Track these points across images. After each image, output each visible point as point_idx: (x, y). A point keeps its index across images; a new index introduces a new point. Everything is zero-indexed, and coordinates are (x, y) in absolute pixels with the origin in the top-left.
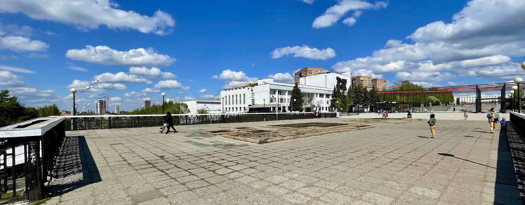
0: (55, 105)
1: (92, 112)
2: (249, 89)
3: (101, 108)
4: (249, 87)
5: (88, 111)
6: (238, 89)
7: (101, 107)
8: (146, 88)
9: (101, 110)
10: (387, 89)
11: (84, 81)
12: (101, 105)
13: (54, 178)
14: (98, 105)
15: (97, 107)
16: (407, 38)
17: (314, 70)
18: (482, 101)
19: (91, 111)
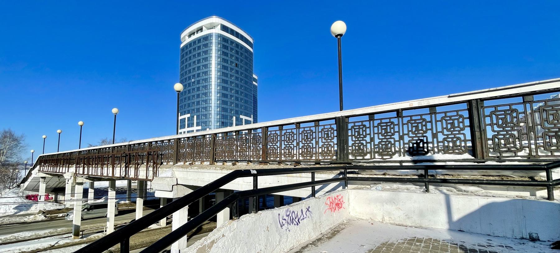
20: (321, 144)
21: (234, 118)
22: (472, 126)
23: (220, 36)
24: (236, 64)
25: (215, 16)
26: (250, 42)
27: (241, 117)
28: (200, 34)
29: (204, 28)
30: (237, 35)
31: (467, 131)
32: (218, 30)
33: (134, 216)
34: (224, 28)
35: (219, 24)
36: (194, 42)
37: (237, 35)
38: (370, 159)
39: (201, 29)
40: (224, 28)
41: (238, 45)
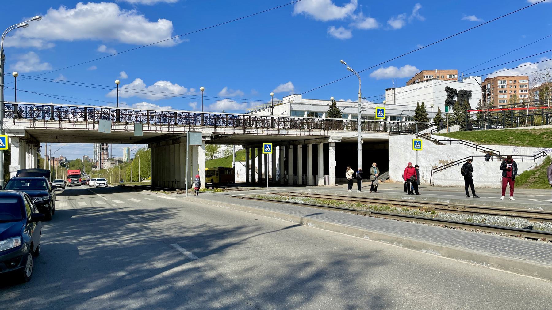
0: (440, 160)
1: (90, 160)
2: (268, 110)
3: (100, 152)
4: (268, 109)
5: (84, 157)
6: (262, 111)
7: (101, 151)
8: (278, 85)
9: (100, 156)
10: (538, 165)
11: (12, 291)
12: (101, 147)
13: (44, 185)
14: (97, 148)
15: (96, 151)
16: (469, 185)
17: (493, 143)
18: (214, 128)
19: (88, 158)
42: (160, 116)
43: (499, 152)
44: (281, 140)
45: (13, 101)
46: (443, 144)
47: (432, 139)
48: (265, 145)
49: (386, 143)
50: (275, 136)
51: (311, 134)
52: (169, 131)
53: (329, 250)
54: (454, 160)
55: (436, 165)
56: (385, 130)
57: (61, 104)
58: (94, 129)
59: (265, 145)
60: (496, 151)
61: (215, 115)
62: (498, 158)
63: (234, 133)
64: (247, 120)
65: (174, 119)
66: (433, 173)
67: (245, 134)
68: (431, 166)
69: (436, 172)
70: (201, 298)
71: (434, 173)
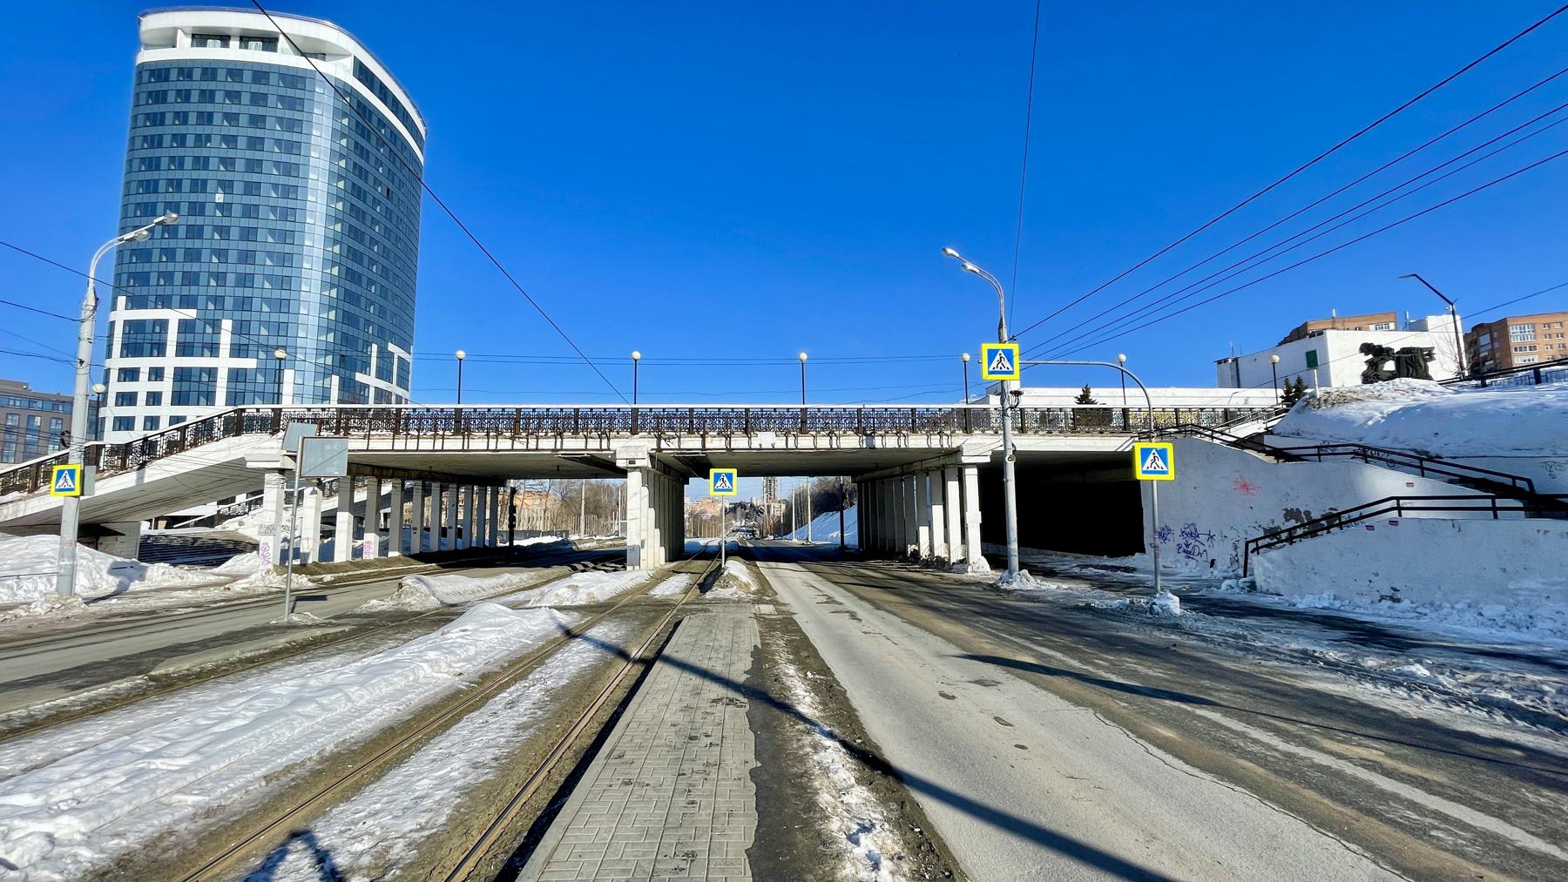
20: (593, 422)
21: (375, 347)
22: (1021, 418)
23: (342, 91)
24: (388, 190)
25: (329, 23)
26: (418, 131)
27: (391, 347)
28: (255, 55)
29: (282, 43)
30: (384, 94)
31: (1020, 420)
32: (341, 71)
33: (1417, 375)
34: (362, 73)
35: (350, 55)
36: (210, 70)
37: (384, 94)
38: (485, 450)
39: (269, 41)
40: (362, 73)
41: (395, 134)
42: (772, 418)
43: (1529, 481)
44: (496, 476)
45: (800, 404)
46: (1298, 458)
47: (1267, 449)
48: (715, 474)
49: (1123, 461)
50: (477, 459)
51: (604, 446)
52: (555, 450)
53: (817, 784)
54: (1336, 510)
55: (1276, 525)
56: (1126, 428)
57: (489, 404)
58: (527, 450)
59: (715, 474)
60: (1514, 478)
61: (534, 410)
62: (1521, 505)
63: (704, 448)
64: (569, 418)
65: (573, 423)
66: (1252, 552)
67: (729, 450)
68: (1260, 526)
69: (1261, 550)
70: (1419, 673)
71: (1255, 553)
